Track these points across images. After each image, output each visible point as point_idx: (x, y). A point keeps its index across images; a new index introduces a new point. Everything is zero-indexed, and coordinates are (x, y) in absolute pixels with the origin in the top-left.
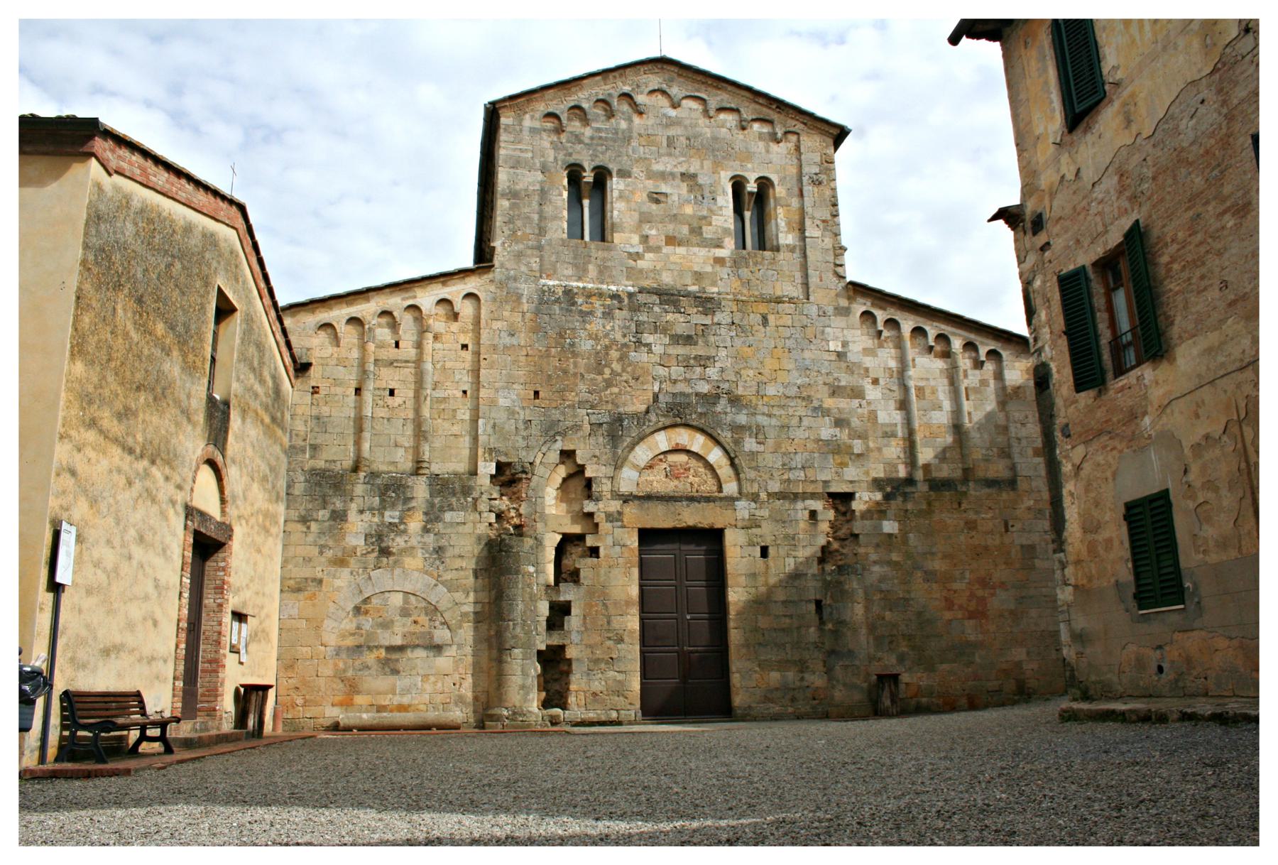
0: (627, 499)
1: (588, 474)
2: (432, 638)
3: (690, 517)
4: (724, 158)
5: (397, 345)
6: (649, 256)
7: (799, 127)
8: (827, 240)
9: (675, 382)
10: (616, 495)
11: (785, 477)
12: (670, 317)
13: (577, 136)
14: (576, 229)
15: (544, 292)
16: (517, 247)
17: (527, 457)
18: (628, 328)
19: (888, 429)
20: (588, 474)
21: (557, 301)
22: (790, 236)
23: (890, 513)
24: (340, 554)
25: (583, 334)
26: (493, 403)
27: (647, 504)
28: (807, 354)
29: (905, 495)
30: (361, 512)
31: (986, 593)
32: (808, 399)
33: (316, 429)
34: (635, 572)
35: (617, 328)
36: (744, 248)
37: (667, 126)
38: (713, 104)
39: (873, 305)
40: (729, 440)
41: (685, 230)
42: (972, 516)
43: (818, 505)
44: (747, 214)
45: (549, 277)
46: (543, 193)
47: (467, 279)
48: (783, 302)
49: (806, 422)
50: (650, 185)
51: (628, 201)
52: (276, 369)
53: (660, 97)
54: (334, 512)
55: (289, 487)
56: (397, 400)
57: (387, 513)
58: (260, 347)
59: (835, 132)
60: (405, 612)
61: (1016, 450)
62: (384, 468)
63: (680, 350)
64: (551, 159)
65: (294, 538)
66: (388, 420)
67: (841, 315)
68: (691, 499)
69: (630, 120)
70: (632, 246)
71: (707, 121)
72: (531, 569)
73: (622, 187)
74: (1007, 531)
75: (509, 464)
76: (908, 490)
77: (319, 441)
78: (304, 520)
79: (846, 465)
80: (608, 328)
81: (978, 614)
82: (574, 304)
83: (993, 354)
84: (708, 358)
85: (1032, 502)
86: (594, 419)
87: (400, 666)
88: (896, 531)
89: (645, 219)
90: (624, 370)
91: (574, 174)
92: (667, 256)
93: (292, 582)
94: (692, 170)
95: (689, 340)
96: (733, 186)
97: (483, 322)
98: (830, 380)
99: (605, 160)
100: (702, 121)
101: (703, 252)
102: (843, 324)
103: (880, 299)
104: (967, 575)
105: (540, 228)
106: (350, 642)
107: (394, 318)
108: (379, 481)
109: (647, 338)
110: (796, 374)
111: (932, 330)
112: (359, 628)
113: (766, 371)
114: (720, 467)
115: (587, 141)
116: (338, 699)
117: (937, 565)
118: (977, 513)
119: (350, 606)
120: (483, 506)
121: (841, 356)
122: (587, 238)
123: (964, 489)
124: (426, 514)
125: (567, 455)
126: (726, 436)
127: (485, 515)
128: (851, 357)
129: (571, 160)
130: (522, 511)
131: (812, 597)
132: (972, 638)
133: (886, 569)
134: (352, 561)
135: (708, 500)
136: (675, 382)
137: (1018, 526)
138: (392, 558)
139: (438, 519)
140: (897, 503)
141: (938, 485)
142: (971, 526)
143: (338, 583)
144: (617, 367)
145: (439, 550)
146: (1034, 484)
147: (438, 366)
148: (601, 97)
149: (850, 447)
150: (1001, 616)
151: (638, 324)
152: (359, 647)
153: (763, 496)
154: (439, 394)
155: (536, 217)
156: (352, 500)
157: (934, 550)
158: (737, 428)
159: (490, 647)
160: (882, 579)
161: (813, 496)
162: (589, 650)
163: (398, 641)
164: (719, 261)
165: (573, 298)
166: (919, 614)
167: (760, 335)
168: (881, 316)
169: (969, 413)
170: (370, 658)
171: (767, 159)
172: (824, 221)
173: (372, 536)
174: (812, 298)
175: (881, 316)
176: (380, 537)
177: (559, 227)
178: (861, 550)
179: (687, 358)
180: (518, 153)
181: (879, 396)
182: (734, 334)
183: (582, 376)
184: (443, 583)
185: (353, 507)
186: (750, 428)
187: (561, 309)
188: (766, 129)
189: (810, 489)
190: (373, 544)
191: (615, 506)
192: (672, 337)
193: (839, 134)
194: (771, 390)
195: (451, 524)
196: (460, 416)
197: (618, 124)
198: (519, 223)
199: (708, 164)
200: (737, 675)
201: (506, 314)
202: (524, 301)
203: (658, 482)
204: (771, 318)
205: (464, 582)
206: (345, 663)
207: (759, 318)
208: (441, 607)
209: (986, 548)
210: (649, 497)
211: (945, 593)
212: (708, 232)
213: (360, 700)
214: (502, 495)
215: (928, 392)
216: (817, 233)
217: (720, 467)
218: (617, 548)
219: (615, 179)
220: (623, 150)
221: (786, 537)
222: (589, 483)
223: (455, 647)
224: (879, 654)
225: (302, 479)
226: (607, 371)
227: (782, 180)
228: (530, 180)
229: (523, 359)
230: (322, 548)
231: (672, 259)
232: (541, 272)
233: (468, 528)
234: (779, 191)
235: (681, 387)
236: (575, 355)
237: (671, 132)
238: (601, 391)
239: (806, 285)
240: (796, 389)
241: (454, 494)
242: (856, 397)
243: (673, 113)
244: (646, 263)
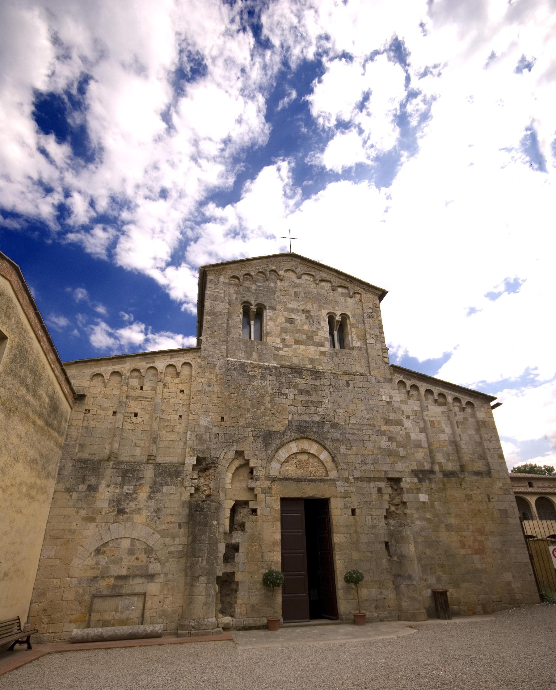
1: (251, 465)
2: (147, 569)
4: (323, 303)
5: (142, 388)
6: (286, 349)
7: (361, 291)
8: (378, 345)
9: (300, 415)
10: (268, 477)
11: (363, 468)
12: (297, 380)
13: (248, 288)
15: (228, 364)
16: (213, 340)
18: (275, 385)
19: (417, 443)
20: (251, 465)
21: (235, 369)
22: (359, 343)
23: (423, 490)
24: (90, 514)
28: (371, 402)
29: (430, 479)
30: (108, 486)
31: (482, 538)
32: (373, 426)
33: (85, 435)
34: (279, 524)
36: (334, 347)
37: (294, 287)
38: (318, 278)
39: (404, 377)
40: (331, 447)
41: (305, 337)
42: (469, 492)
43: (382, 485)
44: (336, 333)
45: (231, 357)
47: (185, 355)
48: (357, 375)
49: (373, 438)
52: (54, 392)
53: (291, 273)
54: (89, 486)
56: (139, 419)
57: (125, 487)
58: (36, 373)
59: (380, 293)
60: (131, 552)
61: (488, 455)
62: (127, 459)
63: (304, 398)
64: (234, 298)
66: (132, 430)
67: (388, 382)
68: (311, 480)
69: (276, 283)
71: (315, 285)
72: (215, 523)
73: (271, 314)
74: (490, 501)
75: (205, 458)
79: (396, 462)
80: (264, 384)
81: (480, 551)
82: (245, 371)
83: (469, 403)
84: (318, 402)
85: (501, 485)
88: (427, 500)
89: (284, 330)
90: (272, 407)
92: (295, 350)
94: (308, 309)
96: (329, 318)
97: (193, 378)
100: (313, 286)
101: (314, 348)
103: (407, 375)
104: (471, 527)
105: (227, 332)
106: (90, 574)
107: (141, 373)
109: (286, 391)
110: (365, 412)
111: (436, 390)
112: (97, 564)
113: (350, 410)
114: (327, 462)
117: (452, 521)
118: (471, 490)
120: (187, 483)
121: (389, 403)
122: (252, 338)
123: (462, 476)
124: (151, 487)
125: (239, 454)
126: (329, 444)
129: (245, 300)
130: (211, 486)
132: (479, 566)
133: (424, 523)
134: (98, 518)
135: (321, 481)
136: (300, 415)
137: (496, 498)
138: (125, 516)
139: (158, 491)
140: (426, 484)
141: (448, 474)
142: (469, 498)
143: (86, 533)
144: (269, 406)
145: (158, 511)
146: (501, 474)
148: (261, 270)
150: (494, 552)
153: (351, 479)
154: (164, 417)
155: (225, 326)
157: (450, 512)
158: (334, 440)
159: (186, 575)
161: (380, 479)
163: (124, 572)
164: (322, 353)
168: (409, 383)
169: (460, 435)
171: (344, 305)
172: (376, 336)
173: (114, 501)
174: (372, 374)
175: (409, 383)
176: (119, 503)
178: (408, 511)
179: (307, 402)
181: (410, 425)
182: (332, 390)
184: (158, 532)
185: (104, 482)
188: (345, 291)
189: (377, 476)
190: (113, 506)
192: (298, 391)
193: (382, 294)
196: (176, 429)
197: (269, 284)
199: (315, 306)
201: (207, 374)
202: (217, 368)
203: (291, 470)
204: (351, 383)
206: (84, 590)
208: (155, 548)
209: (479, 511)
210: (286, 479)
212: (316, 339)
214: (200, 477)
215: (436, 423)
216: (373, 341)
217: (327, 462)
219: (267, 310)
220: (272, 297)
221: (365, 503)
222: (252, 471)
223: (162, 576)
224: (425, 577)
225: (71, 465)
226: (263, 407)
227: (354, 316)
228: (222, 307)
229: (215, 399)
231: (298, 351)
232: (227, 353)
233: (177, 497)
234: (352, 320)
235: (304, 418)
237: (297, 290)
239: (369, 367)
240: (366, 420)
243: (297, 281)
244: (285, 352)
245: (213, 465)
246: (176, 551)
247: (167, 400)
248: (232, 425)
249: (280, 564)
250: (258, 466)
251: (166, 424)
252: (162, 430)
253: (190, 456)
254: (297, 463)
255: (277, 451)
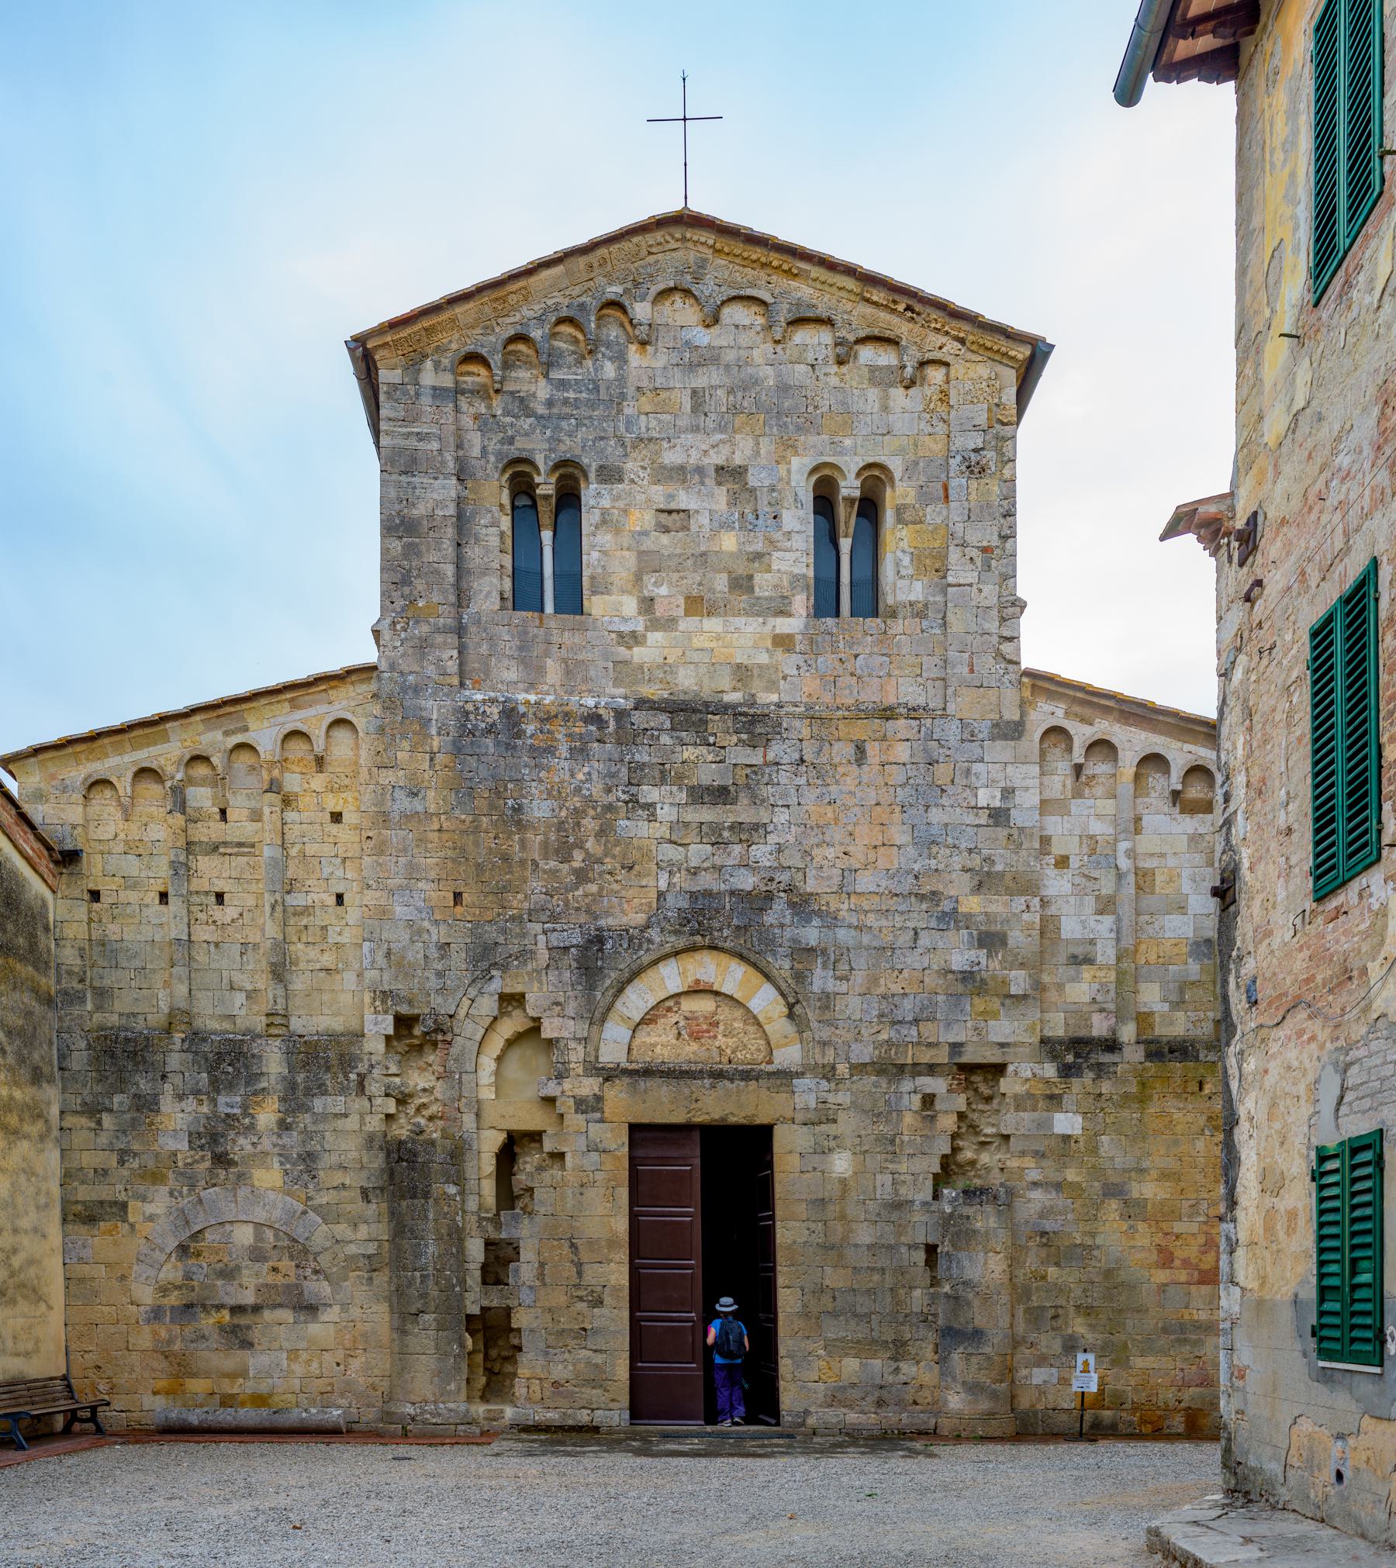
0: (610, 1075)
3: (716, 1105)
6: (655, 637)
8: (987, 589)
10: (594, 1068)
11: (884, 1036)
12: (689, 753)
13: (522, 400)
14: (524, 594)
17: (444, 1005)
19: (1079, 951)
25: (535, 789)
27: (642, 1084)
28: (936, 816)
35: (589, 777)
37: (692, 367)
44: (845, 544)
46: (462, 521)
49: (925, 940)
50: (658, 494)
51: (618, 531)
55: (62, 1057)
57: (222, 1099)
59: (1022, 352)
62: (215, 1025)
63: (706, 814)
64: (476, 452)
65: (79, 1139)
66: (217, 945)
67: (1005, 737)
69: (621, 359)
70: (625, 620)
72: (452, 1190)
76: (1106, 1058)
77: (107, 982)
78: (93, 1110)
79: (995, 1016)
80: (581, 776)
82: (520, 734)
84: (756, 827)
86: (555, 940)
87: (255, 1335)
89: (648, 564)
91: (521, 485)
92: (688, 634)
94: (738, 460)
95: (721, 795)
98: (976, 861)
99: (569, 447)
102: (1007, 756)
106: (174, 1299)
108: (206, 1048)
109: (650, 793)
110: (911, 851)
112: (188, 1276)
114: (770, 1020)
115: (541, 410)
116: (162, 1384)
117: (1148, 1190)
119: (172, 1244)
120: (374, 1088)
121: (999, 816)
122: (549, 608)
127: (379, 1101)
128: (1018, 818)
129: (513, 452)
131: (921, 1239)
143: (150, 1209)
145: (309, 1158)
147: (293, 852)
148: (564, 313)
149: (1005, 983)
151: (636, 768)
152: (189, 1306)
155: (449, 570)
156: (164, 1077)
158: (804, 953)
160: (1045, 1213)
161: (932, 1069)
162: (548, 1317)
163: (249, 1298)
164: (783, 642)
165: (517, 724)
166: (1108, 1273)
167: (850, 783)
170: (208, 1322)
172: (985, 550)
176: (214, 1138)
177: (489, 590)
179: (716, 828)
180: (413, 443)
181: (1067, 888)
182: (802, 781)
183: (535, 863)
186: (824, 952)
187: (498, 744)
188: (886, 357)
189: (926, 1057)
190: (202, 1147)
191: (589, 1086)
194: (866, 882)
198: (420, 584)
200: (789, 1361)
202: (434, 731)
203: (662, 1044)
204: (873, 750)
205: (349, 1207)
206: (169, 1331)
207: (849, 750)
210: (647, 1072)
211: (1159, 1239)
212: (764, 584)
213: (198, 1386)
218: (594, 1156)
223: (337, 1309)
225: (83, 1044)
227: (910, 469)
230: (123, 1155)
232: (462, 674)
235: (707, 881)
236: (521, 826)
237: (701, 380)
238: (567, 891)
240: (911, 879)
241: (328, 1069)
242: (1021, 893)
243: (703, 337)
244: (654, 648)
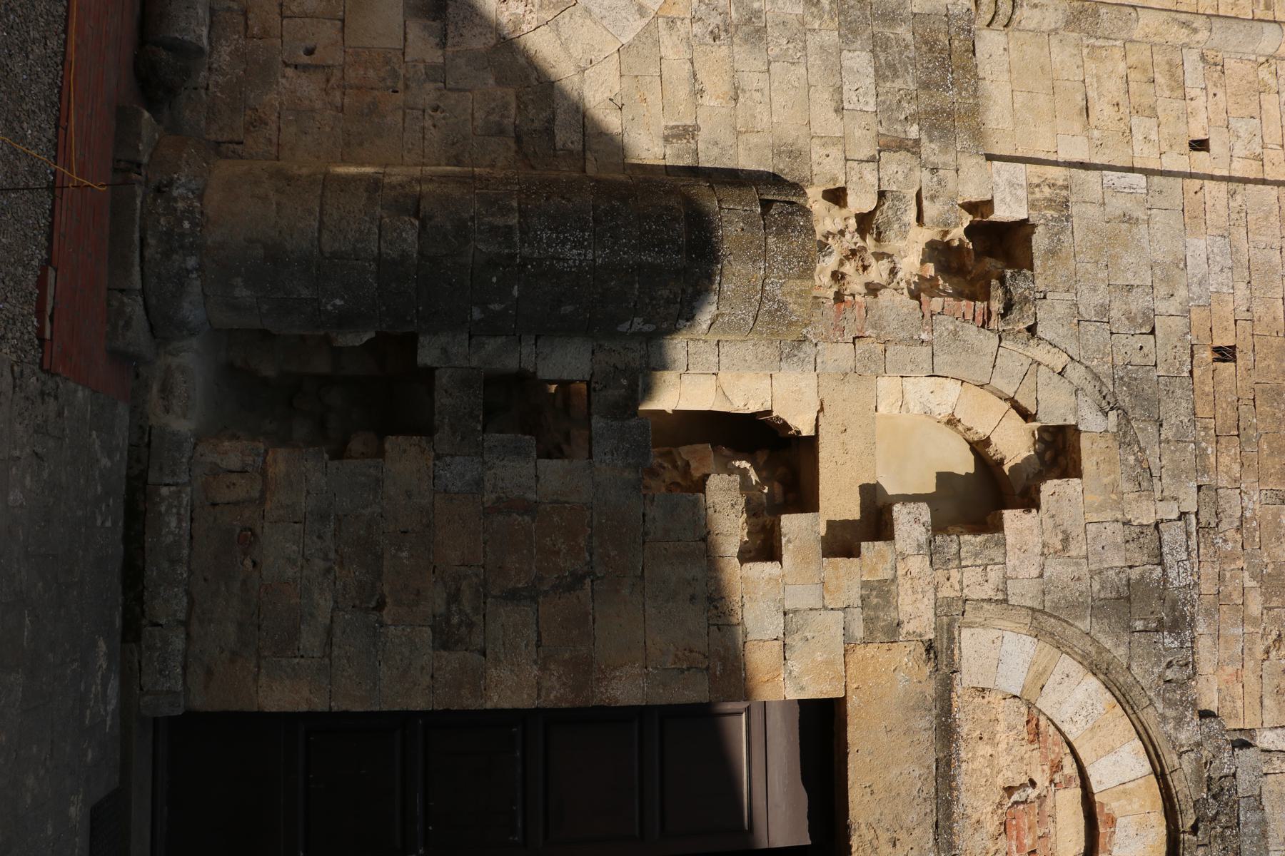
0: (940, 652)
1: (1012, 518)
10: (951, 617)
26: (1191, 217)
27: (924, 723)
93: (163, 509)
120: (895, 169)
125: (1059, 451)
130: (885, 296)
147: (1264, 73)
154: (1193, 73)
184: (648, 36)
191: (916, 612)
195: (837, 70)
196: (1141, 125)
203: (994, 759)
205: (654, 98)
210: (946, 732)
223: (436, 57)
245: (996, 306)
246: (552, 120)
247: (1272, 81)
248: (1204, 410)
249: (471, 703)
250: (1012, 561)
251: (1160, 79)
252: (1132, 60)
253: (1031, 187)
254: (1032, 793)
255: (1094, 669)
